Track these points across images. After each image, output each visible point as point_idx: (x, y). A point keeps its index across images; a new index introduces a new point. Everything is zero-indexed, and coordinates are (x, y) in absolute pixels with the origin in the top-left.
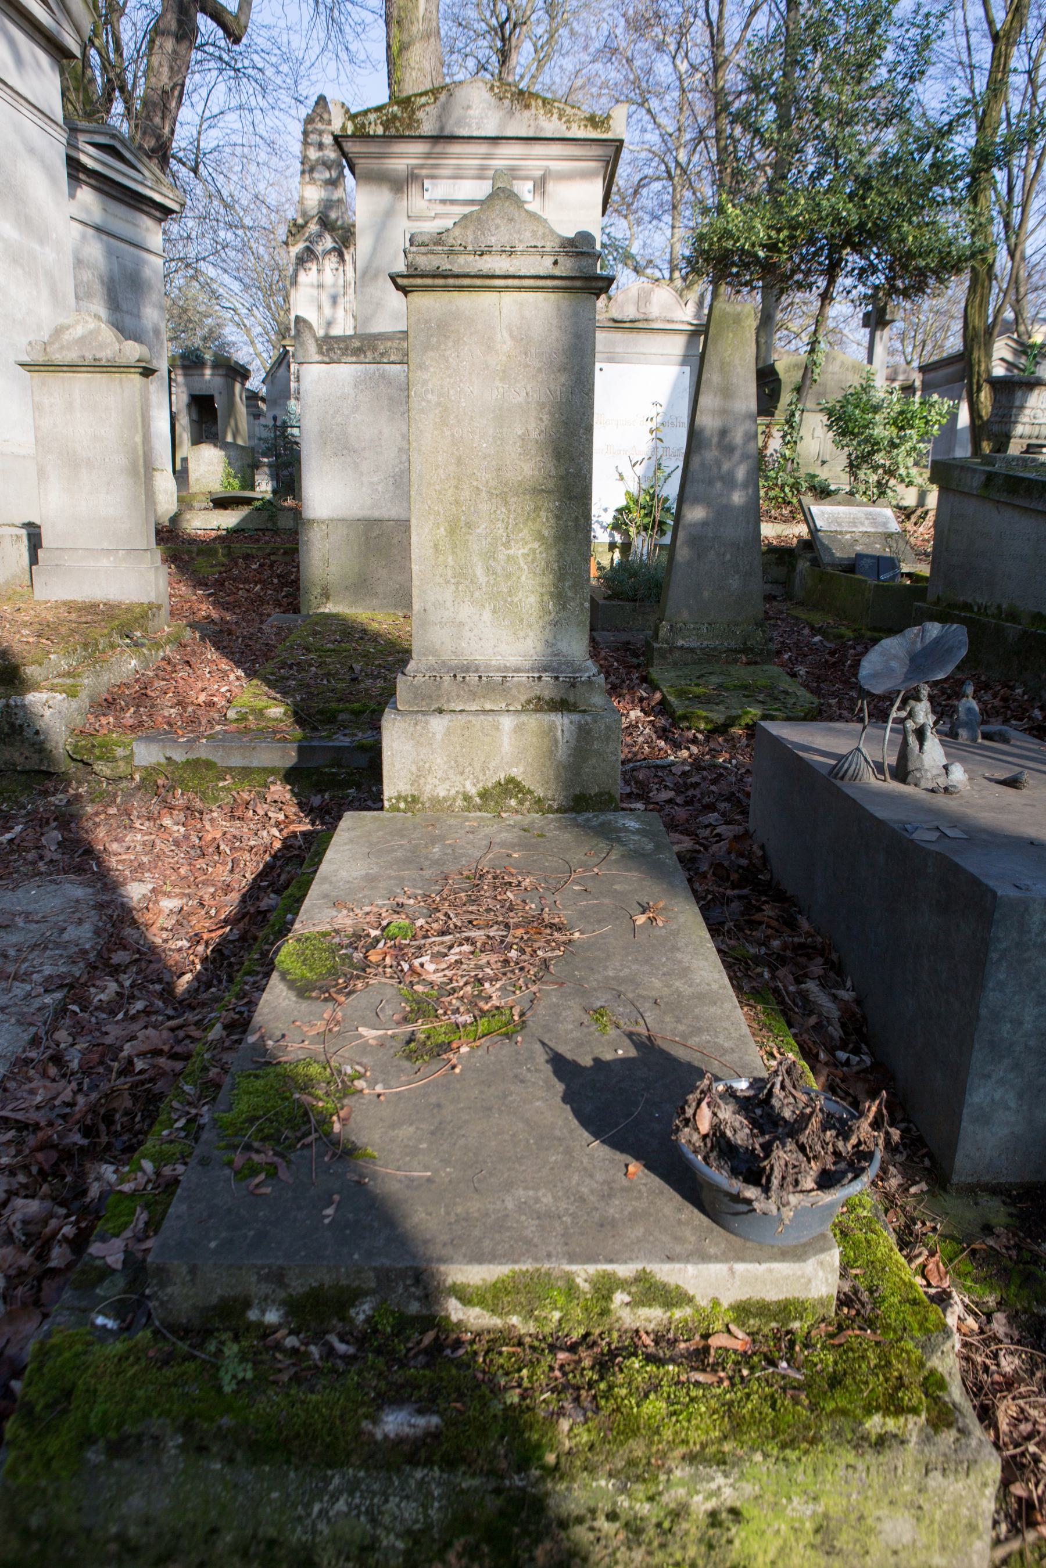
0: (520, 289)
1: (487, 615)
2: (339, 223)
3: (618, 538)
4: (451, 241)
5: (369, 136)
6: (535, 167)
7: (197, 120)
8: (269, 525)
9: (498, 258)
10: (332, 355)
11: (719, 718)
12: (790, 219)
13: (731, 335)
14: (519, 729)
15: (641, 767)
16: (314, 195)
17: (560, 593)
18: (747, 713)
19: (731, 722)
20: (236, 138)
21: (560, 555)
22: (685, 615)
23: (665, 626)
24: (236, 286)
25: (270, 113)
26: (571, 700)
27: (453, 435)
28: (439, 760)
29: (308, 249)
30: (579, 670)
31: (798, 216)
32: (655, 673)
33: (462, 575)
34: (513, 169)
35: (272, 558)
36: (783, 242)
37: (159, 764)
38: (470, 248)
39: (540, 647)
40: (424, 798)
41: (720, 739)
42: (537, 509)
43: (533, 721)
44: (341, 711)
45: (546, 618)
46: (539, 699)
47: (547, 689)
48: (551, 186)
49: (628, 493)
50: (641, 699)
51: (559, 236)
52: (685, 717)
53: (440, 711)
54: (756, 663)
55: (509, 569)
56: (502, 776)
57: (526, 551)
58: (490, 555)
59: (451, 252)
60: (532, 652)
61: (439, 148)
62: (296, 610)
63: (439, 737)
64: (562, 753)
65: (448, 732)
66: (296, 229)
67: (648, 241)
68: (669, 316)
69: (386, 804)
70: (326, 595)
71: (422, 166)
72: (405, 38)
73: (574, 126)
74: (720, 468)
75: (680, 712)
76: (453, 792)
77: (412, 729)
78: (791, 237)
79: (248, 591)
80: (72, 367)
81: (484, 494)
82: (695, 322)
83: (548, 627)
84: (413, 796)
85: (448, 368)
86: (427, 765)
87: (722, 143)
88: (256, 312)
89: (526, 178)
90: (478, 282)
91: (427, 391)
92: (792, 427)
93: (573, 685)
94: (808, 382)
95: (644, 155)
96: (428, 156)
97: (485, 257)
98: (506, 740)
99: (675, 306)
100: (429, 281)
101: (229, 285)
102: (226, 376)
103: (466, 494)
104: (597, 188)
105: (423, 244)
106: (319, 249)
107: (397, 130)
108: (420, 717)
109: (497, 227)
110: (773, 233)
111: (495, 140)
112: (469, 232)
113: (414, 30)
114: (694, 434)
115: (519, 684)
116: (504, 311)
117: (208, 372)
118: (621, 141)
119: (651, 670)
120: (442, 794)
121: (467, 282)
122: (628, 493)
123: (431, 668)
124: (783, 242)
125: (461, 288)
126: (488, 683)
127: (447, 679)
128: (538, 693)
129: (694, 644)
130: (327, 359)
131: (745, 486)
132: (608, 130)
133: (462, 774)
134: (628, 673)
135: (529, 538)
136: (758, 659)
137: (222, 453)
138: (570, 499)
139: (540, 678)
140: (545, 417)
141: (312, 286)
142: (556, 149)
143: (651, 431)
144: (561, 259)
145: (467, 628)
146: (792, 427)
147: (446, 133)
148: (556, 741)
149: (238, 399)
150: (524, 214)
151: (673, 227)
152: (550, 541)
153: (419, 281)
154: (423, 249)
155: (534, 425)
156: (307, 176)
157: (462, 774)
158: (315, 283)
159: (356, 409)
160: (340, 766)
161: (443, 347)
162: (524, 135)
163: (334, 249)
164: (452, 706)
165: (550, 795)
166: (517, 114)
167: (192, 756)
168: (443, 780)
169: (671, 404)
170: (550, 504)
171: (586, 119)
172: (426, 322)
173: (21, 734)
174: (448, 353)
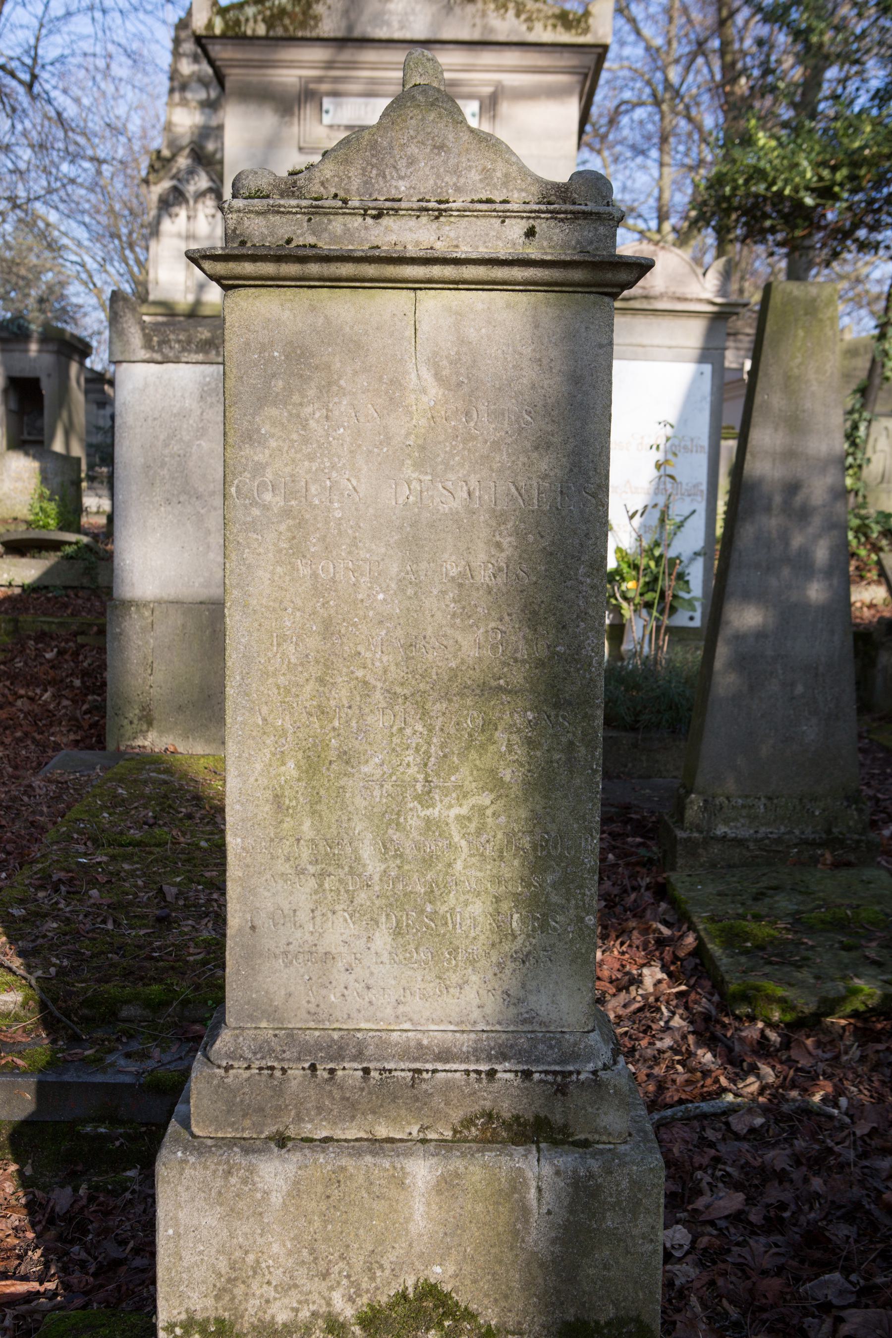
0: (456, 284)
1: (382, 940)
4: (316, 188)
5: (245, 37)
7: (35, 23)
8: (85, 581)
9: (412, 222)
10: (166, 350)
11: (807, 1005)
12: (851, 154)
13: (801, 333)
14: (446, 1186)
15: (673, 1119)
16: (186, 120)
17: (535, 897)
18: (855, 992)
19: (830, 1006)
20: (86, 46)
21: (536, 818)
22: (731, 785)
23: (695, 801)
24: (82, 234)
25: (132, 16)
26: (558, 1118)
27: (315, 575)
28: (276, 1248)
29: (175, 189)
30: (574, 1056)
31: (862, 148)
32: (679, 880)
33: (331, 859)
35: (80, 639)
36: (841, 185)
38: (354, 203)
39: (493, 1004)
41: (809, 1042)
42: (489, 726)
43: (482, 1170)
44: (127, 1002)
45: (507, 947)
46: (489, 1116)
47: (506, 1091)
48: (504, 107)
50: (661, 942)
51: (538, 180)
52: (744, 997)
53: (282, 1141)
54: (848, 865)
55: (430, 846)
56: (410, 1282)
57: (464, 811)
58: (389, 818)
59: (315, 211)
60: (476, 1014)
61: (347, 55)
62: (101, 744)
63: (276, 1199)
64: (537, 1236)
65: (296, 1191)
66: (160, 163)
67: (629, 183)
68: (680, 291)
70: (148, 720)
71: (320, 80)
73: (538, 26)
74: (787, 544)
75: (733, 988)
76: (305, 1314)
77: (219, 1183)
78: (852, 178)
79: (32, 699)
81: (378, 695)
82: (719, 300)
83: (510, 965)
84: (220, 1321)
85: (306, 441)
86: (251, 1258)
87: (729, 58)
88: (109, 268)
89: (470, 97)
90: (371, 270)
91: (262, 486)
92: (854, 444)
93: (561, 1090)
94: (877, 381)
95: (626, 73)
96: (330, 65)
97: (385, 221)
99: (684, 275)
100: (268, 268)
101: (72, 232)
102: (59, 353)
103: (341, 694)
104: (571, 109)
105: (259, 195)
106: (191, 189)
107: (286, 29)
108: (237, 1157)
109: (412, 161)
110: (826, 173)
111: (426, 43)
112: (353, 172)
114: (741, 486)
115: (449, 1086)
116: (424, 328)
117: (34, 347)
118: (605, 48)
119: (674, 877)
121: (346, 269)
123: (263, 1049)
124: (841, 185)
125: (335, 283)
126: (382, 1083)
127: (296, 1073)
128: (488, 1104)
129: (745, 833)
130: (158, 357)
131: (829, 572)
132: (586, 31)
133: (325, 1276)
134: (633, 876)
135: (470, 785)
136: (852, 858)
137: (36, 465)
138: (557, 706)
139: (492, 1073)
140: (506, 542)
141: (179, 236)
142: (511, 58)
143: (658, 466)
144: (541, 226)
145: (340, 965)
146: (854, 444)
147: (357, 34)
148: (525, 1210)
149: (73, 383)
150: (466, 137)
151: (662, 165)
152: (516, 790)
153: (248, 268)
154: (258, 204)
155: (482, 556)
157: (325, 1276)
158: (184, 232)
159: (201, 432)
160: (115, 1121)
161: (296, 398)
162: (465, 35)
163: (210, 190)
164: (308, 1129)
165: (511, 1321)
166: (458, 10)
168: (284, 1289)
169: (685, 418)
170: (515, 716)
171: (555, 16)
172: (263, 348)
174: (309, 409)
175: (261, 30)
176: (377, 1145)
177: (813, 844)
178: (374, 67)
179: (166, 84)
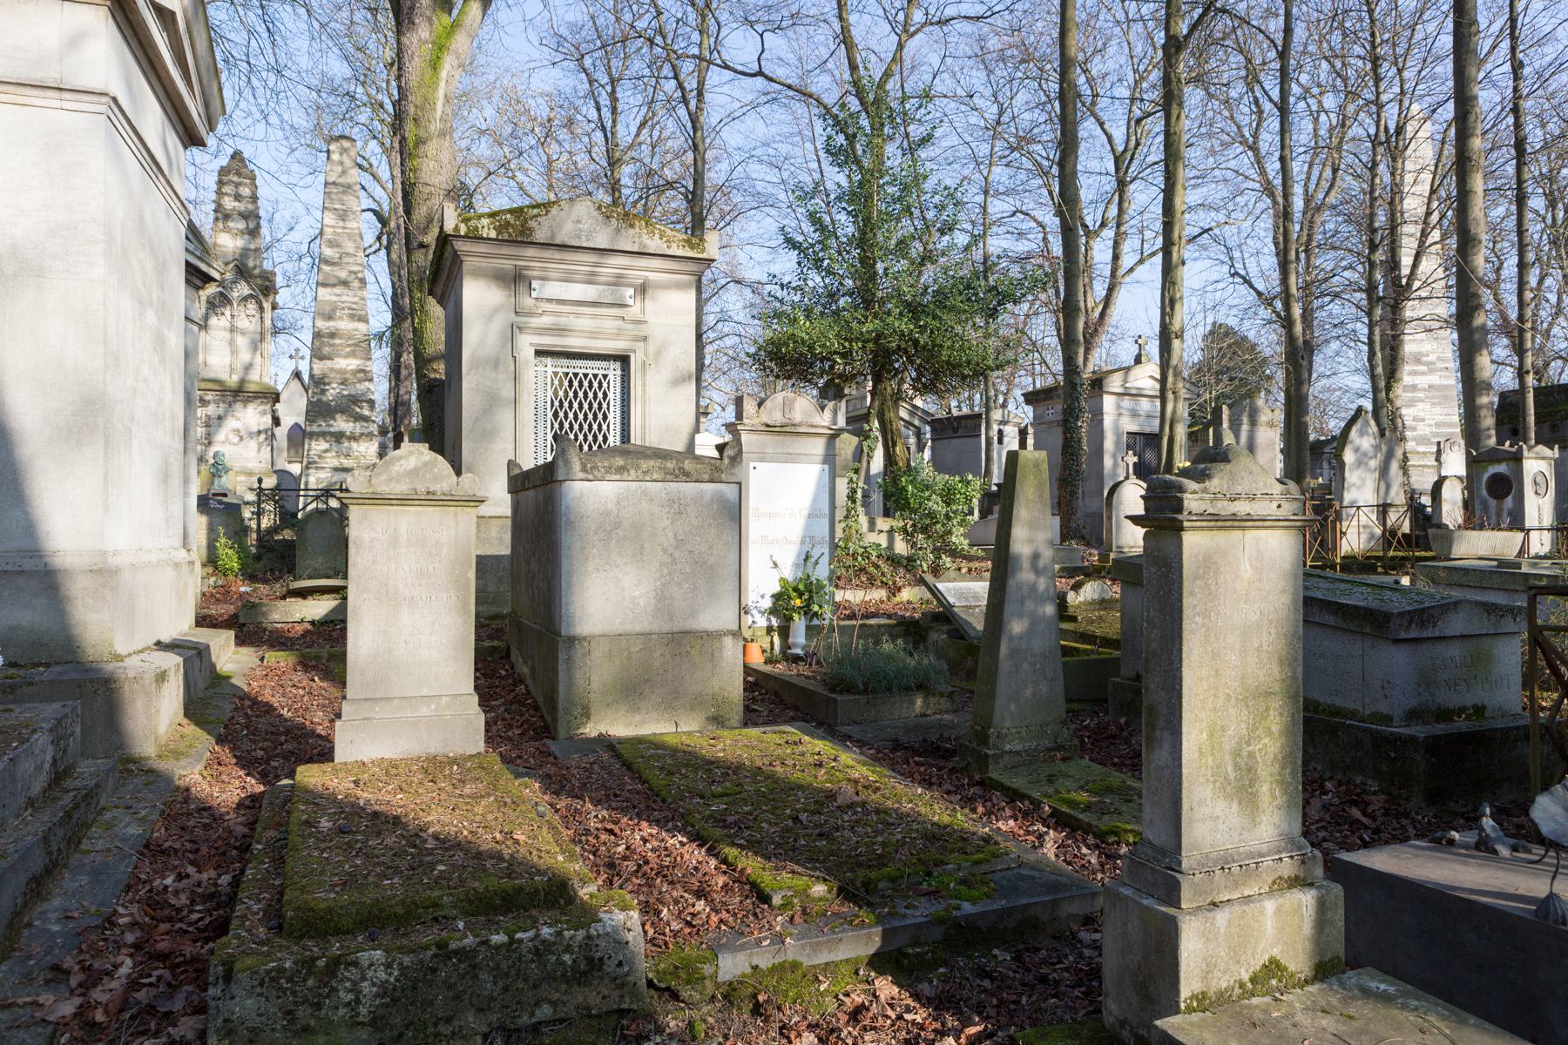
2: (257, 271)
3: (775, 622)
6: (637, 276)
34: (620, 276)
37: (744, 975)
40: (1211, 993)
49: (782, 579)
69: (1183, 1006)
72: (422, 133)
73: (674, 245)
80: (403, 501)
89: (629, 285)
98: (1269, 923)
113: (432, 128)
120: (1224, 985)
122: (782, 579)
129: (1019, 748)
156: (221, 225)
167: (778, 960)
169: (815, 499)
173: (601, 969)
175: (493, 234)
176: (1247, 899)
177: (1048, 749)
178: (574, 263)
179: (212, 216)
